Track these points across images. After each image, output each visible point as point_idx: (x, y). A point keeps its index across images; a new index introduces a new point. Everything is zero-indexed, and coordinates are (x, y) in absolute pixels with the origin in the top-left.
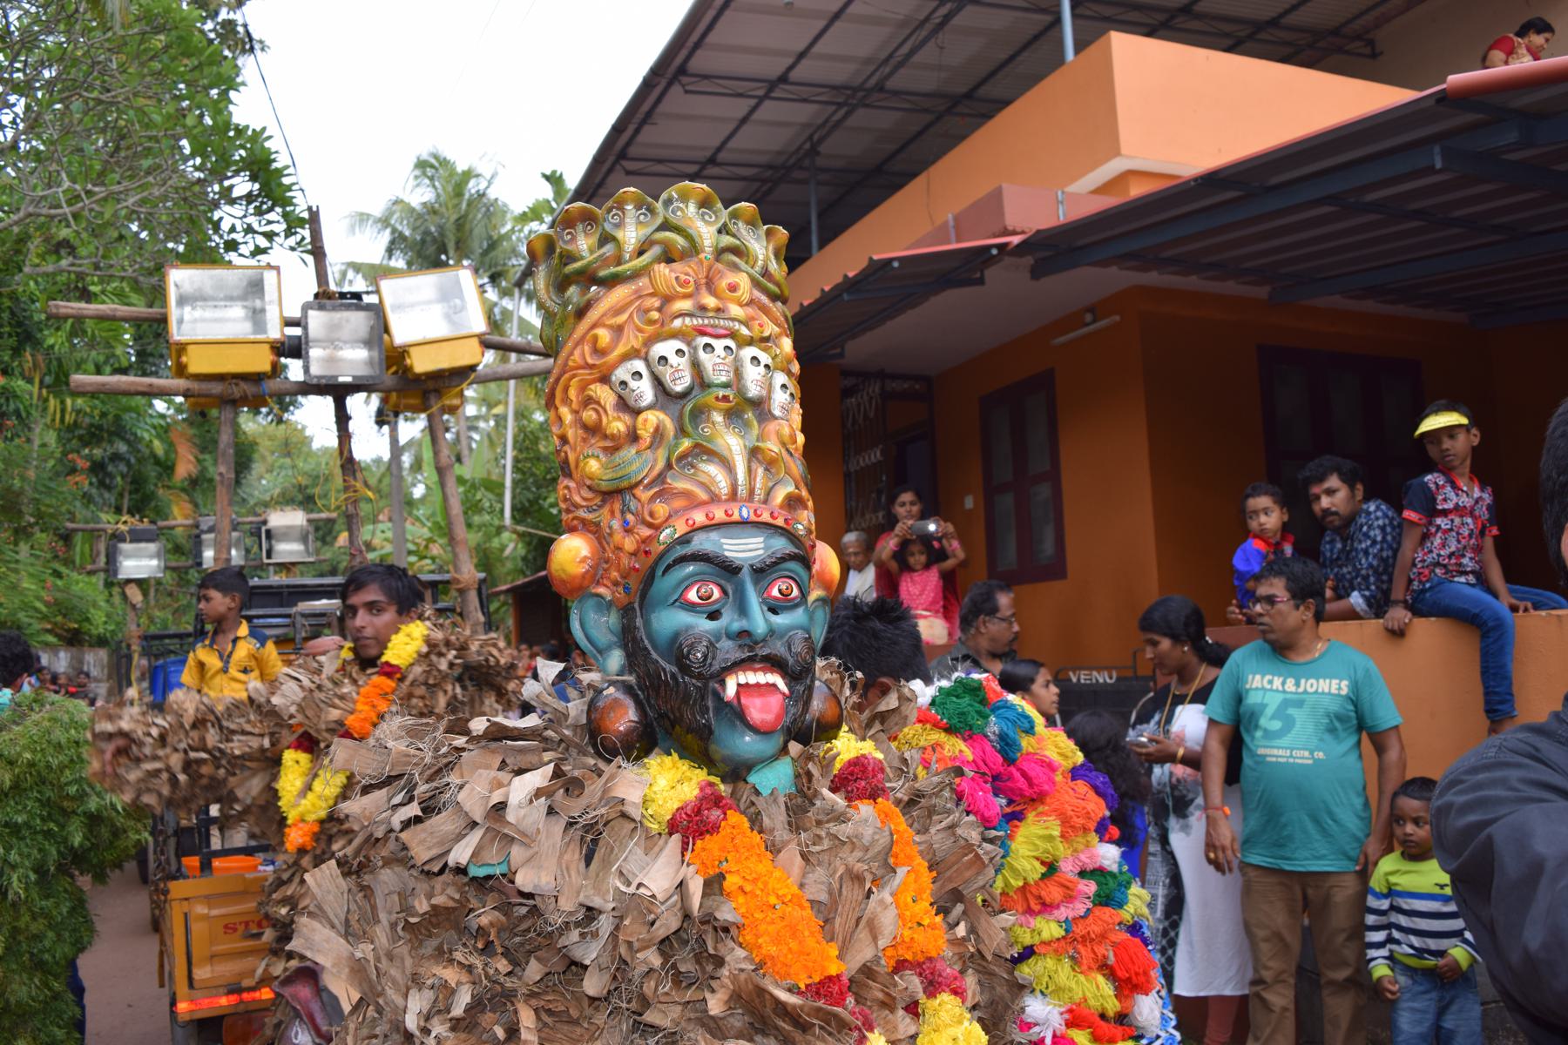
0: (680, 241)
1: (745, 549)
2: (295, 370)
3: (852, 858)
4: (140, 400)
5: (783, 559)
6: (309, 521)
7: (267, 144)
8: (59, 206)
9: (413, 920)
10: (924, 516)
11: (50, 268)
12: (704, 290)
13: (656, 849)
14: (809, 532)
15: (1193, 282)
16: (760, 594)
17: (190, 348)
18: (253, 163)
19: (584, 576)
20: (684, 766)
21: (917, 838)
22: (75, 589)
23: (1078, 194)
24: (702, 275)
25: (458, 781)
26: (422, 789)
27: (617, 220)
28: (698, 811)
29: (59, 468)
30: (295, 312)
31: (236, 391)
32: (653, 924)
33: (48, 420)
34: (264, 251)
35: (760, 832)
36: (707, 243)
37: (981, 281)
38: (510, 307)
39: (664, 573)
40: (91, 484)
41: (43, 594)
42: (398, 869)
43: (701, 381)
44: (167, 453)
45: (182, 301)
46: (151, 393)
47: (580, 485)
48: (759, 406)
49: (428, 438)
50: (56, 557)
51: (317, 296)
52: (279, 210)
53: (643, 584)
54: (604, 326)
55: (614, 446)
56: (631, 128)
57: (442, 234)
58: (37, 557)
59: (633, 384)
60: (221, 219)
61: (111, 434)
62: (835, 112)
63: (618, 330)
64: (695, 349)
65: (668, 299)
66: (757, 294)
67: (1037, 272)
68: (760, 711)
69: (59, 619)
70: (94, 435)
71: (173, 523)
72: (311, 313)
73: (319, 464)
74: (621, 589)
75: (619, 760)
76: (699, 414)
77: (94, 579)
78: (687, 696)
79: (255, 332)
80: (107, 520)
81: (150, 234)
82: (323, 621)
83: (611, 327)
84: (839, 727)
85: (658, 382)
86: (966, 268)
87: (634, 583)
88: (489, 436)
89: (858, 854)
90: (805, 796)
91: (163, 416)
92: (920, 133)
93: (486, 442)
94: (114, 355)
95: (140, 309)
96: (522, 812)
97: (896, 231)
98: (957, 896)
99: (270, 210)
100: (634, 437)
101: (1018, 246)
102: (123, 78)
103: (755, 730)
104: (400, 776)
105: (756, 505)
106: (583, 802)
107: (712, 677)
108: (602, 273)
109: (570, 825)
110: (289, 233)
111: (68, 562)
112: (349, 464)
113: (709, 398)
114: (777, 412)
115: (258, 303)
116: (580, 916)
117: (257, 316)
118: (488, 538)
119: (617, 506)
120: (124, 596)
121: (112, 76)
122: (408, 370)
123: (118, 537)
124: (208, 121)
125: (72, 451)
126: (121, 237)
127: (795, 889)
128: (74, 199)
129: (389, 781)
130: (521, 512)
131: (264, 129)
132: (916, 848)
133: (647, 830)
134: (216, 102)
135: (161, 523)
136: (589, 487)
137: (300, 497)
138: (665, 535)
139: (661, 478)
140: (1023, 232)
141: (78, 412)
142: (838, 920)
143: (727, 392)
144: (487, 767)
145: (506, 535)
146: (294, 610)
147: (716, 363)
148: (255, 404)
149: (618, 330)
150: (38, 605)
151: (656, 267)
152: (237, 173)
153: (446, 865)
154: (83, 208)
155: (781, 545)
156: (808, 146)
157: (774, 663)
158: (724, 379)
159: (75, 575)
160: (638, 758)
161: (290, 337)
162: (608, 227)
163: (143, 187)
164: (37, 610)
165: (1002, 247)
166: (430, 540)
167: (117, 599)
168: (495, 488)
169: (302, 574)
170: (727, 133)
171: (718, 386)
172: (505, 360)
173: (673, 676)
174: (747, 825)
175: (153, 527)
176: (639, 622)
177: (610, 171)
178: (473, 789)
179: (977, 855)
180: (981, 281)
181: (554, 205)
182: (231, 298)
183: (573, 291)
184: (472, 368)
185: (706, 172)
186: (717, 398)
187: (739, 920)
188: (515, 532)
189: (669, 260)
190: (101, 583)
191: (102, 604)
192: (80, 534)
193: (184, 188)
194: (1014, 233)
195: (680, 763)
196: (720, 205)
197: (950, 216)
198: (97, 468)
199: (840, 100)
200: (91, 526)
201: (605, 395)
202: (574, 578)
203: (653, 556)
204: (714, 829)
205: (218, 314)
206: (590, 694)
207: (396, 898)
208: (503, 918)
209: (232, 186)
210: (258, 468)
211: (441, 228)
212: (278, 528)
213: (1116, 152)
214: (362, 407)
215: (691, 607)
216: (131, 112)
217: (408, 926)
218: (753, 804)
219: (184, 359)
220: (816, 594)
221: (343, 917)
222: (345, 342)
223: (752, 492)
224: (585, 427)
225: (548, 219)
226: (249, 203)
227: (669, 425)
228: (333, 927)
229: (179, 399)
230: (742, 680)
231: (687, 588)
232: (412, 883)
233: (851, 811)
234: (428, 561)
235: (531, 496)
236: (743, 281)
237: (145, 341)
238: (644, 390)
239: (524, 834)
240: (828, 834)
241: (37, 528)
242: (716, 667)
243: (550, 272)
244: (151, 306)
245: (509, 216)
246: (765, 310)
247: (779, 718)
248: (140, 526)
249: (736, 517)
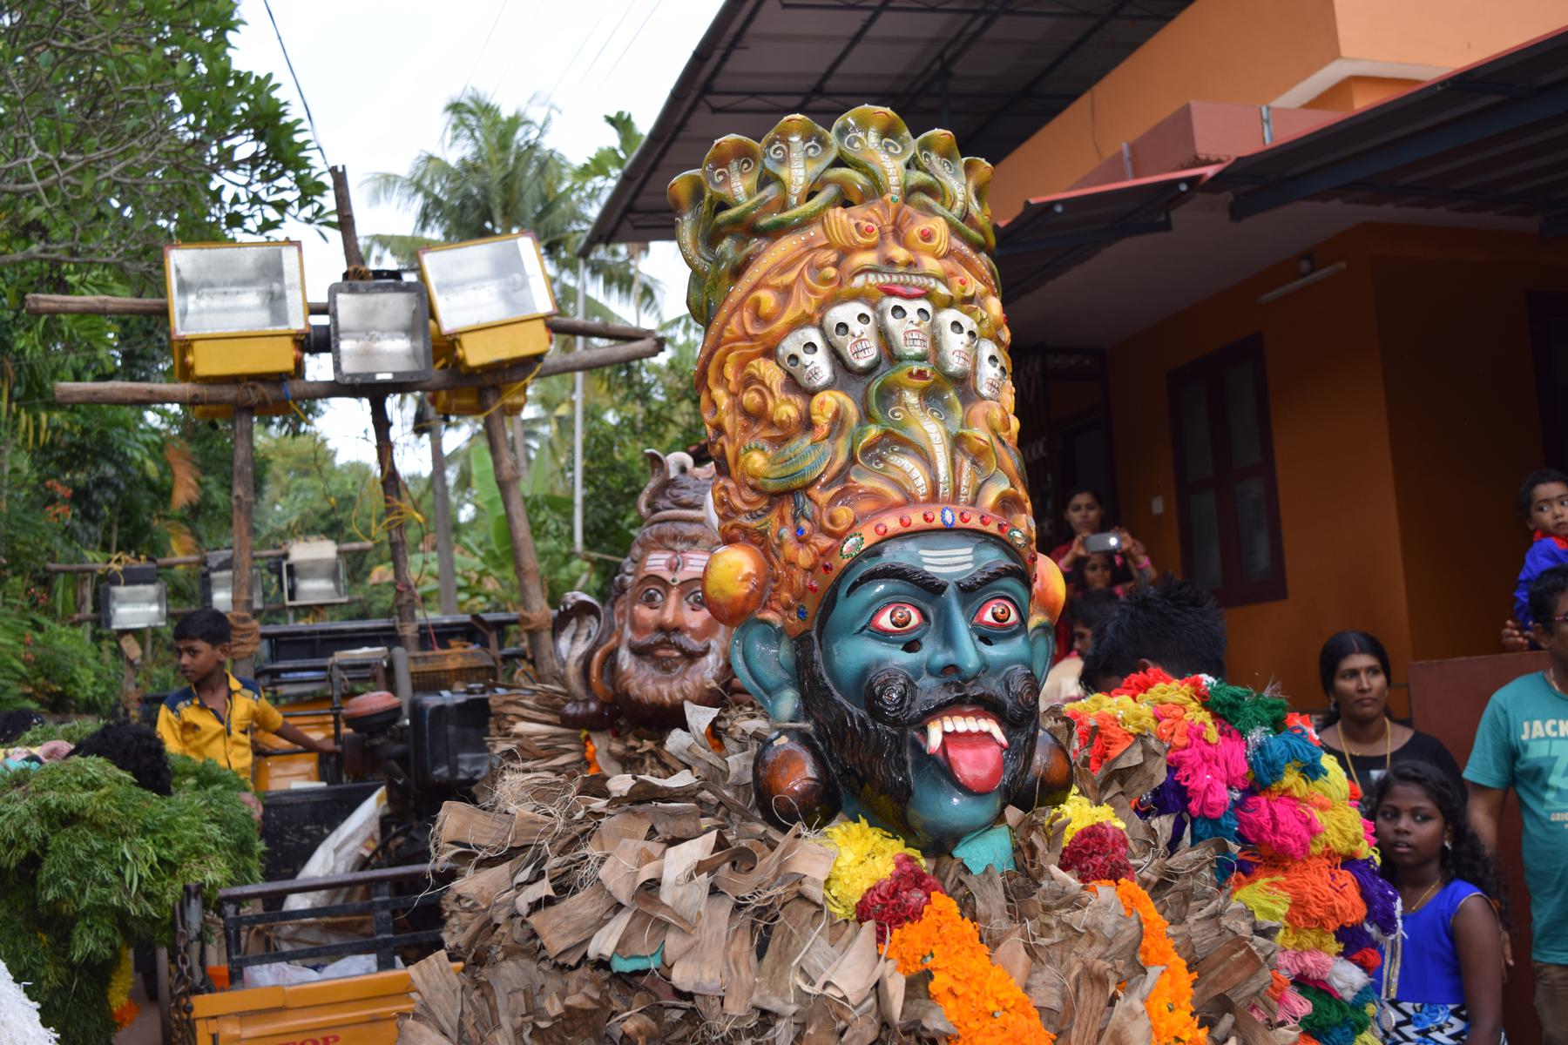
0: (859, 179)
1: (950, 562)
2: (319, 368)
3: (1091, 954)
4: (128, 412)
5: (997, 575)
6: (339, 552)
7: (274, 95)
8: (28, 180)
9: (543, 1025)
10: (1104, 526)
11: (19, 256)
12: (890, 240)
13: (844, 939)
14: (1029, 540)
15: (1439, 215)
16: (969, 620)
17: (197, 345)
18: (257, 118)
19: (747, 598)
20: (875, 836)
21: (1171, 930)
22: (58, 643)
23: (1289, 108)
24: (888, 222)
25: (599, 854)
26: (553, 862)
27: (780, 155)
28: (894, 892)
29: (37, 498)
30: (321, 298)
31: (253, 396)
32: (842, 1034)
33: (20, 440)
34: (274, 225)
35: (974, 919)
36: (893, 180)
37: (1166, 226)
38: (571, 282)
39: (849, 592)
40: (74, 516)
41: (21, 650)
42: (524, 962)
43: (889, 354)
44: (162, 475)
45: (184, 287)
46: (145, 403)
47: (741, 485)
48: (964, 384)
49: (483, 444)
50: (34, 606)
51: (346, 276)
52: (291, 174)
53: (822, 607)
54: (767, 286)
55: (782, 436)
56: (717, 54)
57: (486, 197)
58: (12, 606)
59: (806, 358)
60: (222, 188)
61: (95, 454)
62: (971, 22)
63: (786, 292)
64: (882, 313)
65: (845, 252)
66: (956, 243)
67: (1238, 212)
68: (972, 765)
69: (40, 680)
70: (76, 456)
71: (175, 559)
72: (340, 297)
73: (343, 484)
74: (794, 614)
75: (799, 827)
76: (888, 394)
77: (80, 632)
78: (880, 747)
79: (274, 323)
80: (94, 559)
81: (135, 208)
82: (367, 673)
83: (776, 288)
84: (1068, 789)
85: (836, 355)
86: (1148, 209)
87: (810, 605)
88: (550, 444)
89: (1098, 949)
90: (1028, 875)
91: (156, 431)
92: (1078, 44)
93: (547, 451)
94: (96, 359)
95: (122, 299)
96: (680, 891)
97: (1068, 162)
98: (1224, 1004)
99: (280, 174)
100: (807, 424)
101: (1214, 178)
102: (98, 21)
103: (965, 789)
104: (525, 848)
105: (962, 507)
106: (754, 878)
107: (911, 723)
108: (764, 222)
109: (738, 908)
110: (304, 201)
111: (50, 611)
112: (391, 479)
113: (900, 374)
114: (985, 391)
115: (276, 287)
116: (753, 1022)
117: (275, 301)
118: (554, 568)
119: (788, 511)
120: (118, 652)
121: (85, 20)
122: (459, 362)
123: (111, 579)
124: (202, 69)
125: (49, 477)
126: (100, 215)
127: (1019, 992)
128: (45, 170)
129: (512, 853)
130: (594, 535)
131: (269, 76)
132: (1171, 942)
133: (831, 916)
134: (212, 46)
135: (161, 561)
136: (753, 488)
137: (323, 525)
138: (849, 545)
139: (842, 475)
140: (1219, 161)
141: (55, 429)
142: (1074, 1032)
143: (923, 366)
144: (633, 836)
145: (576, 564)
146: (330, 661)
147: (907, 330)
148: (265, 410)
149: (786, 292)
150: (16, 663)
151: (831, 212)
152: (239, 131)
153: (585, 956)
154: (56, 182)
155: (993, 557)
156: (937, 66)
157: (987, 706)
158: (918, 350)
159: (57, 628)
160: (820, 826)
161: (315, 327)
162: (769, 165)
163: (125, 154)
164: (14, 670)
165: (1192, 181)
166: (483, 573)
167: (107, 656)
168: (562, 506)
169: (332, 619)
170: (836, 54)
171: (911, 359)
172: (567, 348)
173: (862, 722)
174: (957, 910)
175: (151, 565)
176: (817, 654)
177: (693, 108)
178: (617, 863)
179: (1250, 952)
180: (1166, 226)
181: (622, 155)
182: (246, 283)
183: (727, 245)
184: (538, 358)
185: (811, 105)
186: (910, 374)
187: (953, 1030)
188: (588, 559)
189: (847, 204)
190: (88, 636)
191: (90, 660)
192: (62, 576)
193: (176, 152)
194: (1208, 163)
195: (870, 831)
196: (907, 133)
197: (1124, 146)
198: (80, 496)
199: (977, 7)
200: (76, 566)
201: (770, 372)
202: (735, 600)
203: (834, 574)
204: (915, 915)
205: (228, 302)
206: (753, 749)
207: (521, 997)
208: (653, 1024)
209: (233, 148)
210: (271, 490)
211: (484, 189)
212: (301, 563)
213: (1335, 54)
214: (401, 410)
215: (882, 635)
216: (110, 63)
217: (537, 1032)
218: (961, 883)
219: (190, 359)
220: (1036, 620)
221: (455, 1020)
222: (383, 331)
223: (956, 491)
224: (746, 413)
225: (616, 172)
226: (254, 167)
227: (852, 409)
228: (444, 1034)
229: (175, 408)
230: (949, 728)
231: (878, 612)
232: (540, 979)
233: (1088, 894)
234: (482, 599)
235: (607, 515)
236: (939, 227)
237: (133, 340)
238: (819, 366)
239: (682, 919)
240: (1060, 923)
241: (9, 572)
242: (916, 711)
243: (698, 221)
244: (140, 296)
245: (567, 171)
246: (966, 263)
247: (995, 775)
248: (136, 565)
249: (937, 522)
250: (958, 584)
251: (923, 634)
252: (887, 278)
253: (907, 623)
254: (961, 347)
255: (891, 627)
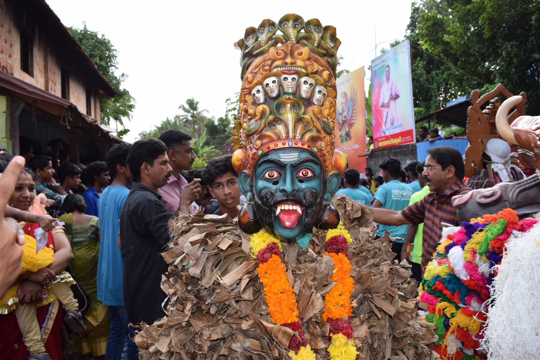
59: (257, 95)
65: (274, 61)
76: (279, 107)
85: (266, 94)
108: (254, 53)
147: (289, 85)
215: (267, 180)
223: (294, 137)
230: (283, 208)
238: (261, 97)
246: (316, 61)
249: (287, 146)
250: (291, 165)
251: (280, 179)
252: (284, 68)
253: (273, 176)
254: (306, 89)
255: (268, 177)
